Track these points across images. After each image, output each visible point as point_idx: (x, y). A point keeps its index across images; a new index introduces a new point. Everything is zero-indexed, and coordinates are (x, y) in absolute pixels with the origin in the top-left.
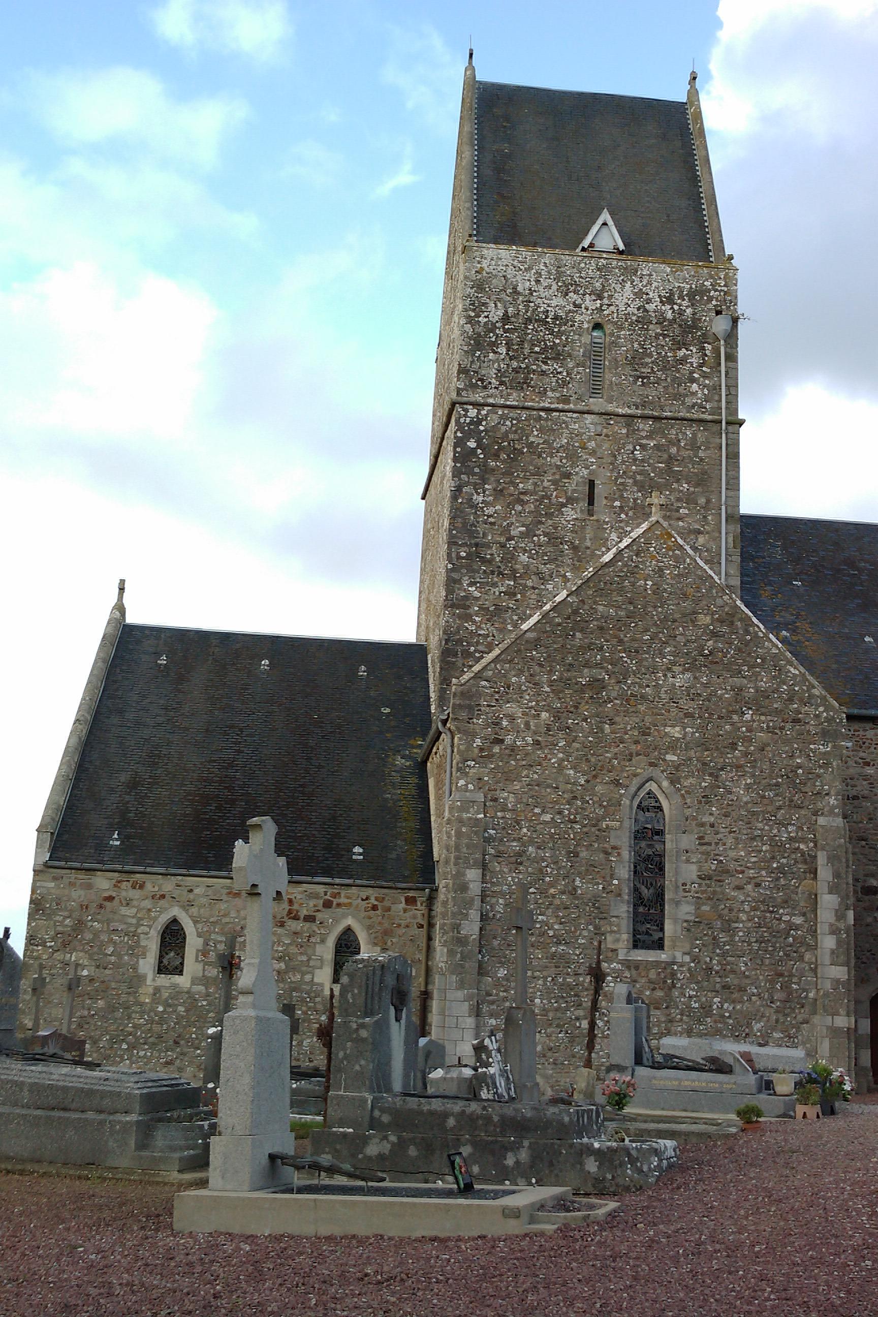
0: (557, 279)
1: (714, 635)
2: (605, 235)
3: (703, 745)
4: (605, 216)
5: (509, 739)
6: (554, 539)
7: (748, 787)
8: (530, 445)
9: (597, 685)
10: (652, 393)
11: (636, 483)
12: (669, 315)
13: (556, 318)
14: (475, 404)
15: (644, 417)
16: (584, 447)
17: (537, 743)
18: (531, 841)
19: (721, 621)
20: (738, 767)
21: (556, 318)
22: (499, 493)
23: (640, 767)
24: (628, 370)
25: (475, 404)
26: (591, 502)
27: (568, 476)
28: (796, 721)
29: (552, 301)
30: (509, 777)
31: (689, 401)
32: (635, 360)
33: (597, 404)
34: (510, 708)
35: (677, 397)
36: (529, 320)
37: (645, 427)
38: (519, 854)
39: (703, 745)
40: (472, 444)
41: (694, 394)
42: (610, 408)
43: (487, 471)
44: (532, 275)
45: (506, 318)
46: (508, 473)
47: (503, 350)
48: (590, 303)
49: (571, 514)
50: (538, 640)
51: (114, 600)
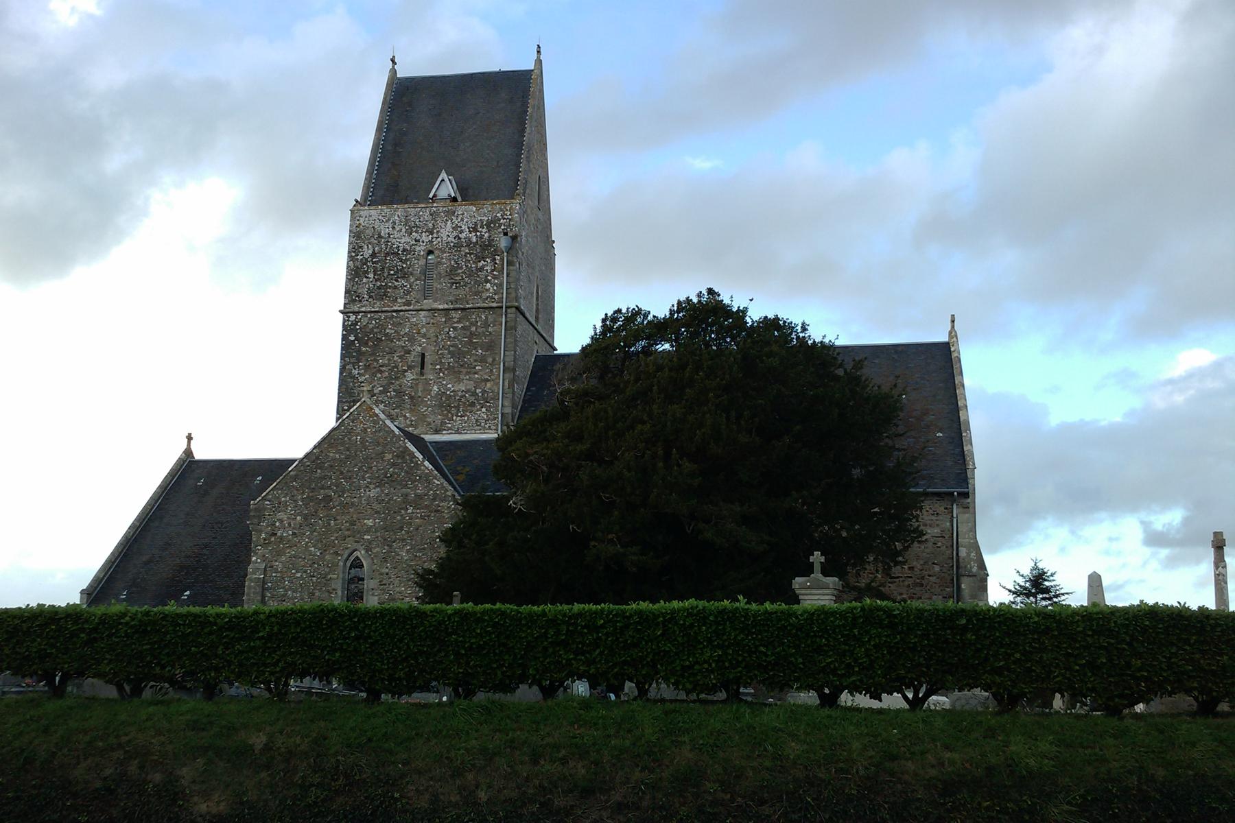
0: (405, 225)
1: (393, 465)
2: (445, 187)
3: (385, 529)
4: (443, 175)
5: (279, 533)
6: (400, 393)
7: (408, 551)
8: (386, 335)
9: (328, 499)
10: (461, 293)
11: (450, 352)
12: (474, 240)
13: (404, 250)
14: (354, 313)
15: (455, 309)
16: (418, 333)
17: (294, 534)
18: (290, 588)
19: (397, 456)
20: (403, 540)
21: (404, 250)
22: (367, 367)
23: (350, 544)
24: (447, 279)
25: (354, 313)
26: (422, 368)
27: (409, 352)
28: (437, 511)
29: (401, 240)
30: (279, 553)
31: (484, 295)
32: (452, 272)
33: (428, 303)
34: (281, 515)
35: (477, 293)
36: (387, 254)
37: (456, 315)
38: (284, 596)
39: (385, 529)
40: (352, 338)
41: (487, 290)
42: (436, 306)
43: (360, 353)
44: (390, 224)
45: (374, 255)
46: (373, 354)
47: (371, 275)
48: (425, 238)
49: (410, 376)
50: (296, 475)
51: (185, 447)
